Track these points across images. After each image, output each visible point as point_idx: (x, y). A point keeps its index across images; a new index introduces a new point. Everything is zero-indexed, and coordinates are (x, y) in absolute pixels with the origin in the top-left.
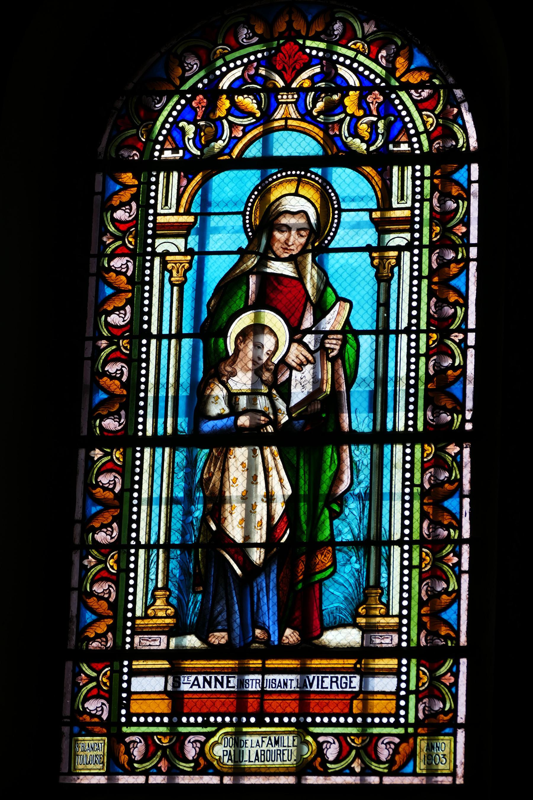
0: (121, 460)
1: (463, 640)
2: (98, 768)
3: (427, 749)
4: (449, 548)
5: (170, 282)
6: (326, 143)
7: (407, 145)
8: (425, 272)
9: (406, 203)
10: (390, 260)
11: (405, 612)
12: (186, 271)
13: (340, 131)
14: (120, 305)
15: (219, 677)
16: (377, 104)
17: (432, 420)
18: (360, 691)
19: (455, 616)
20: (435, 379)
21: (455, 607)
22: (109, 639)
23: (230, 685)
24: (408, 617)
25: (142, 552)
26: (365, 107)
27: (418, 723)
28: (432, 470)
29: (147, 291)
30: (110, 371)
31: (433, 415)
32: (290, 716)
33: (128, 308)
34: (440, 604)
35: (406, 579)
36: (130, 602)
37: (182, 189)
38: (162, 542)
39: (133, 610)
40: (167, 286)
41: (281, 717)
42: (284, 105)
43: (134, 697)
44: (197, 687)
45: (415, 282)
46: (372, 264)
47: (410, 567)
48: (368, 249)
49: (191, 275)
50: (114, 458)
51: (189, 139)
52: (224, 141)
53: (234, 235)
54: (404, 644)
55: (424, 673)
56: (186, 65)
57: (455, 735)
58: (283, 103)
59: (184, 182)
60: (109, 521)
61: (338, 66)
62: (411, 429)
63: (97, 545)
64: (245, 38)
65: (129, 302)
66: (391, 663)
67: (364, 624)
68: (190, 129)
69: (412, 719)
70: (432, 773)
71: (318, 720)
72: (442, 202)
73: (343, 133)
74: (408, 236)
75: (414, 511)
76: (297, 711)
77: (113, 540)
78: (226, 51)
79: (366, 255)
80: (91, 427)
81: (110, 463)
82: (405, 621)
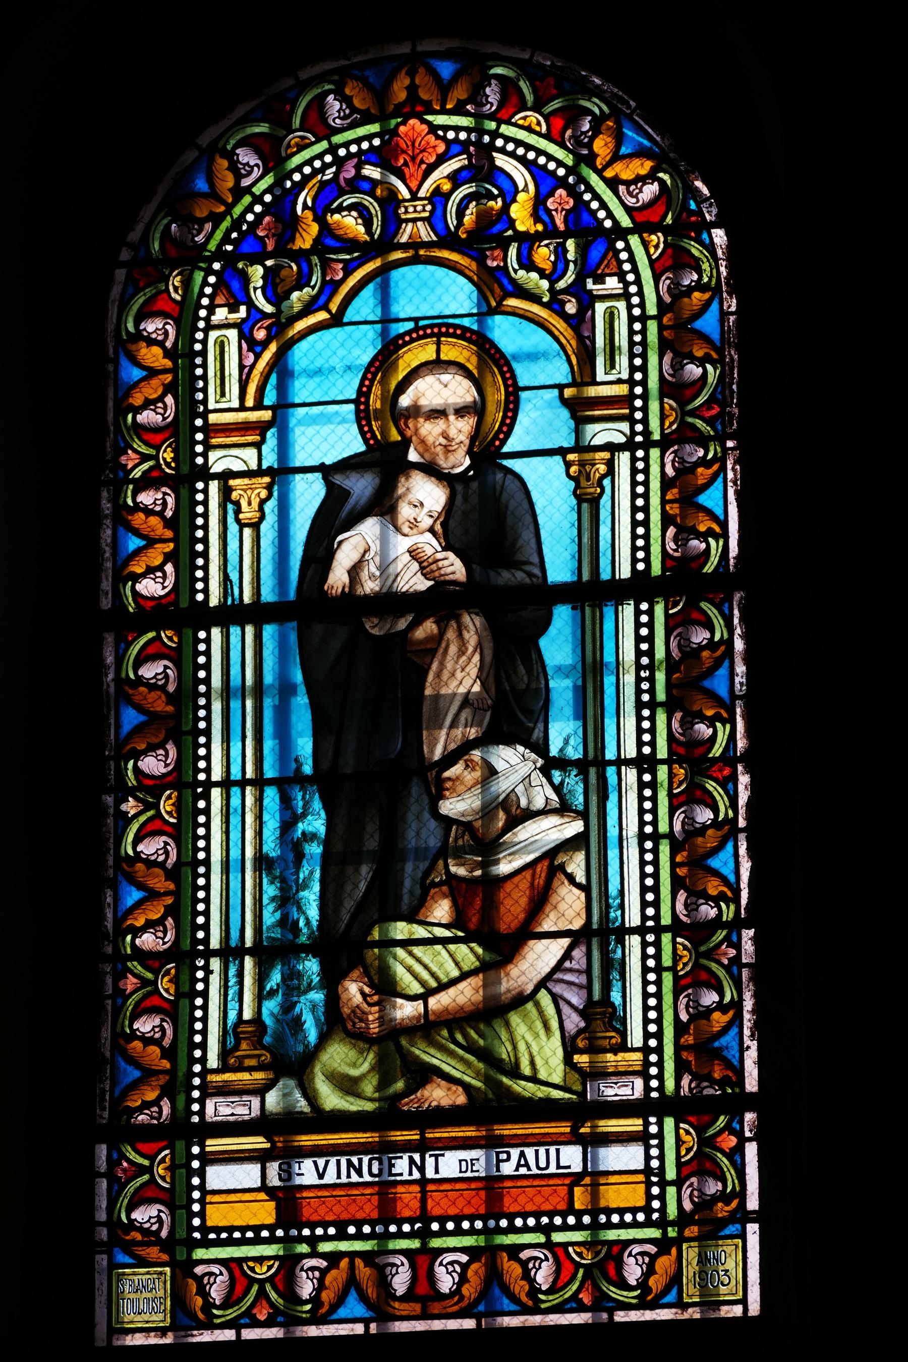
0: (168, 1180)
1: (751, 1084)
2: (158, 1319)
3: (698, 1262)
4: (721, 935)
5: (238, 520)
6: (483, 281)
7: (615, 279)
8: (652, 310)
9: (620, 373)
10: (598, 466)
11: (653, 1043)
12: (262, 502)
13: (505, 259)
14: (155, 396)
15: (355, 1160)
16: (564, 213)
17: (675, 551)
18: (585, 1172)
19: (731, 865)
20: (692, 1027)
21: (734, 1031)
22: (169, 927)
23: (474, 1168)
24: (659, 1050)
25: (215, 964)
26: (546, 218)
27: (683, 1219)
28: (694, 1180)
29: (198, 341)
30: (142, 1030)
31: (681, 726)
32: (472, 1219)
33: (169, 568)
34: (704, 845)
35: (644, 619)
36: (202, 653)
37: (246, 370)
38: (249, 943)
39: (203, 1060)
40: (233, 528)
41: (458, 1220)
42: (410, 225)
43: (209, 1198)
44: (525, 1169)
45: (637, 326)
46: (568, 475)
47: (659, 969)
48: (561, 452)
49: (271, 507)
50: (163, 811)
51: (255, 289)
52: (313, 288)
53: (340, 427)
54: (653, 1120)
55: (688, 1133)
56: (241, 166)
57: (743, 1236)
58: (407, 221)
59: (250, 359)
60: (160, 392)
61: (495, 154)
62: (654, 1095)
63: (140, 954)
64: (339, 117)
65: (169, 389)
66: (634, 1124)
67: (587, 1065)
68: (257, 273)
69: (672, 1211)
70: (710, 1303)
71: (519, 1222)
72: (678, 366)
73: (509, 265)
74: (625, 426)
75: (665, 1024)
76: (482, 1211)
77: (165, 947)
78: (308, 141)
79: (558, 459)
80: (118, 596)
81: (153, 1152)
82: (653, 1058)
